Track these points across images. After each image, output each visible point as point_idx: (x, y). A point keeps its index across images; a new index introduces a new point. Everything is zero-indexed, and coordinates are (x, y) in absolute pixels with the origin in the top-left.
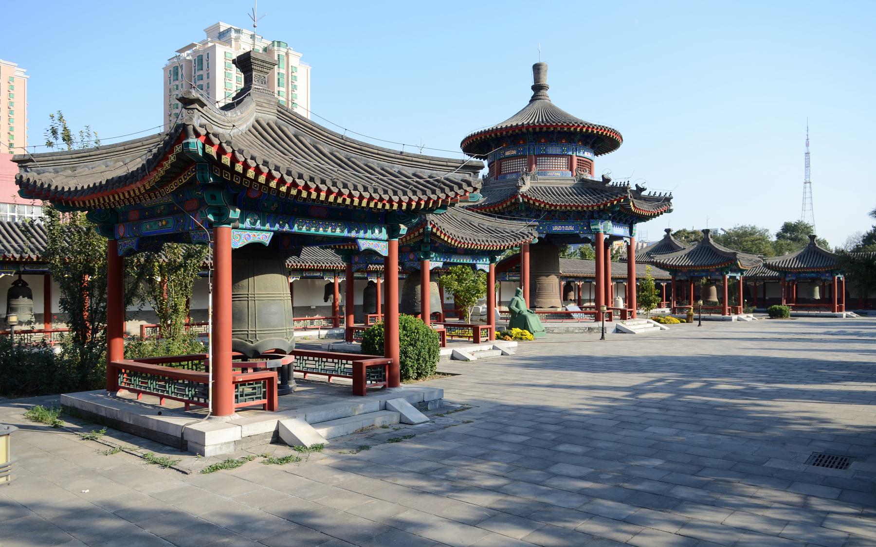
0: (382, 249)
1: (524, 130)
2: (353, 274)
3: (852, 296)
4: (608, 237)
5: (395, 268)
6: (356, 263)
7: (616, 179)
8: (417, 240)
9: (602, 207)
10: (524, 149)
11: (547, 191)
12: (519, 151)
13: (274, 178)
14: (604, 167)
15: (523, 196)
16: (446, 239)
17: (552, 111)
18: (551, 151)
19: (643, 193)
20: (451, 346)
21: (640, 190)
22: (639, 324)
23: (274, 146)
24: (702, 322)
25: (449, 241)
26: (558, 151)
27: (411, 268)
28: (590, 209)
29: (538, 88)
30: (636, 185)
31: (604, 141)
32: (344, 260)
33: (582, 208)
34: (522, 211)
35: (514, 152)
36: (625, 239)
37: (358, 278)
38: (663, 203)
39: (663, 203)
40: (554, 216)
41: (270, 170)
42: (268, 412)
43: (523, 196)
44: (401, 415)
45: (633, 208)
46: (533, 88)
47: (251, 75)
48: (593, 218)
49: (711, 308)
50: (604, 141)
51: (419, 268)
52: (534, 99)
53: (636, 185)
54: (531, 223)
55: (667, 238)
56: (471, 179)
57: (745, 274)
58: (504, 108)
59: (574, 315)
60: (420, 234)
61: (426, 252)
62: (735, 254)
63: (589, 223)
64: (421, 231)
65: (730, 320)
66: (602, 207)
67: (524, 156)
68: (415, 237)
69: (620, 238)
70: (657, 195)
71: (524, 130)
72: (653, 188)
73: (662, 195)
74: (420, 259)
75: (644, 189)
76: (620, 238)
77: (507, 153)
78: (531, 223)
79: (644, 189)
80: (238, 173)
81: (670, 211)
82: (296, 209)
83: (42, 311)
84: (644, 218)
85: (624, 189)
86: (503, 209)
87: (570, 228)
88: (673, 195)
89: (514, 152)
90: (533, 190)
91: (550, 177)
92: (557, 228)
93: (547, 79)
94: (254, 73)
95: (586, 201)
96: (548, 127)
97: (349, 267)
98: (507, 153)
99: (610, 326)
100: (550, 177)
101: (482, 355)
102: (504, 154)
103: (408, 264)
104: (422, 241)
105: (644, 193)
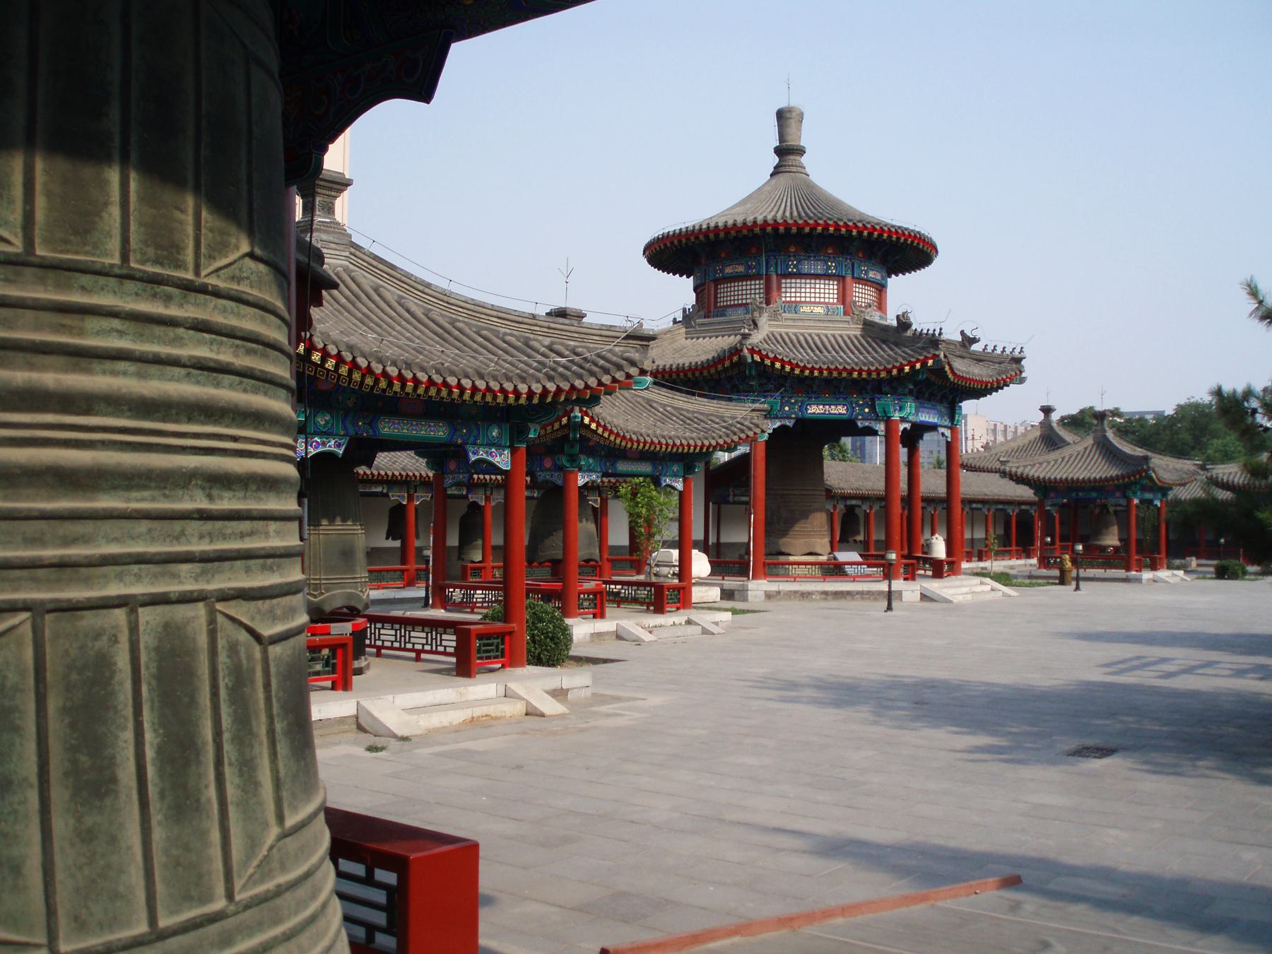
0: (503, 460)
1: (757, 230)
2: (445, 490)
3: (1171, 537)
4: (908, 426)
5: (522, 494)
6: (452, 473)
7: (922, 323)
8: (560, 434)
9: (895, 372)
10: (759, 263)
11: (796, 343)
12: (750, 267)
13: (344, 362)
14: (908, 297)
15: (752, 351)
16: (606, 435)
17: (810, 194)
18: (806, 267)
19: (975, 347)
20: (613, 618)
21: (968, 341)
22: (963, 589)
23: (349, 312)
24: (1082, 584)
25: (612, 438)
26: (820, 268)
27: (546, 482)
28: (874, 375)
29: (787, 151)
30: (962, 333)
31: (907, 252)
32: (430, 465)
33: (860, 374)
34: (751, 377)
35: (741, 269)
36: (941, 430)
37: (454, 497)
38: (1009, 369)
39: (1009, 369)
40: (810, 386)
41: (354, 358)
42: (340, 693)
43: (752, 351)
44: (528, 703)
45: (950, 376)
46: (780, 152)
47: (314, 200)
48: (881, 393)
49: (1098, 557)
50: (907, 252)
51: (560, 482)
52: (777, 171)
53: (962, 333)
54: (757, 406)
55: (1046, 424)
56: (636, 356)
57: (1171, 495)
58: (726, 187)
59: (848, 569)
60: (562, 427)
61: (571, 456)
62: (1146, 459)
63: (873, 400)
64: (565, 420)
65: (1139, 580)
66: (895, 372)
67: (758, 277)
68: (553, 431)
69: (933, 428)
70: (999, 351)
71: (757, 230)
72: (991, 338)
73: (1008, 351)
74: (561, 469)
75: (974, 340)
76: (933, 428)
77: (728, 270)
78: (757, 406)
79: (974, 340)
80: (315, 364)
81: (1022, 381)
82: (380, 404)
83: (883, 538)
84: (980, 390)
85: (933, 341)
86: (718, 373)
87: (839, 410)
88: (1026, 353)
89: (741, 269)
90: (771, 338)
91: (809, 314)
92: (815, 410)
93: (807, 137)
94: (318, 199)
95: (877, 359)
96: (800, 228)
97: (439, 477)
98: (728, 270)
99: (910, 590)
100: (809, 314)
101: (664, 634)
102: (722, 271)
103: (542, 476)
104: (566, 437)
105: (976, 347)
